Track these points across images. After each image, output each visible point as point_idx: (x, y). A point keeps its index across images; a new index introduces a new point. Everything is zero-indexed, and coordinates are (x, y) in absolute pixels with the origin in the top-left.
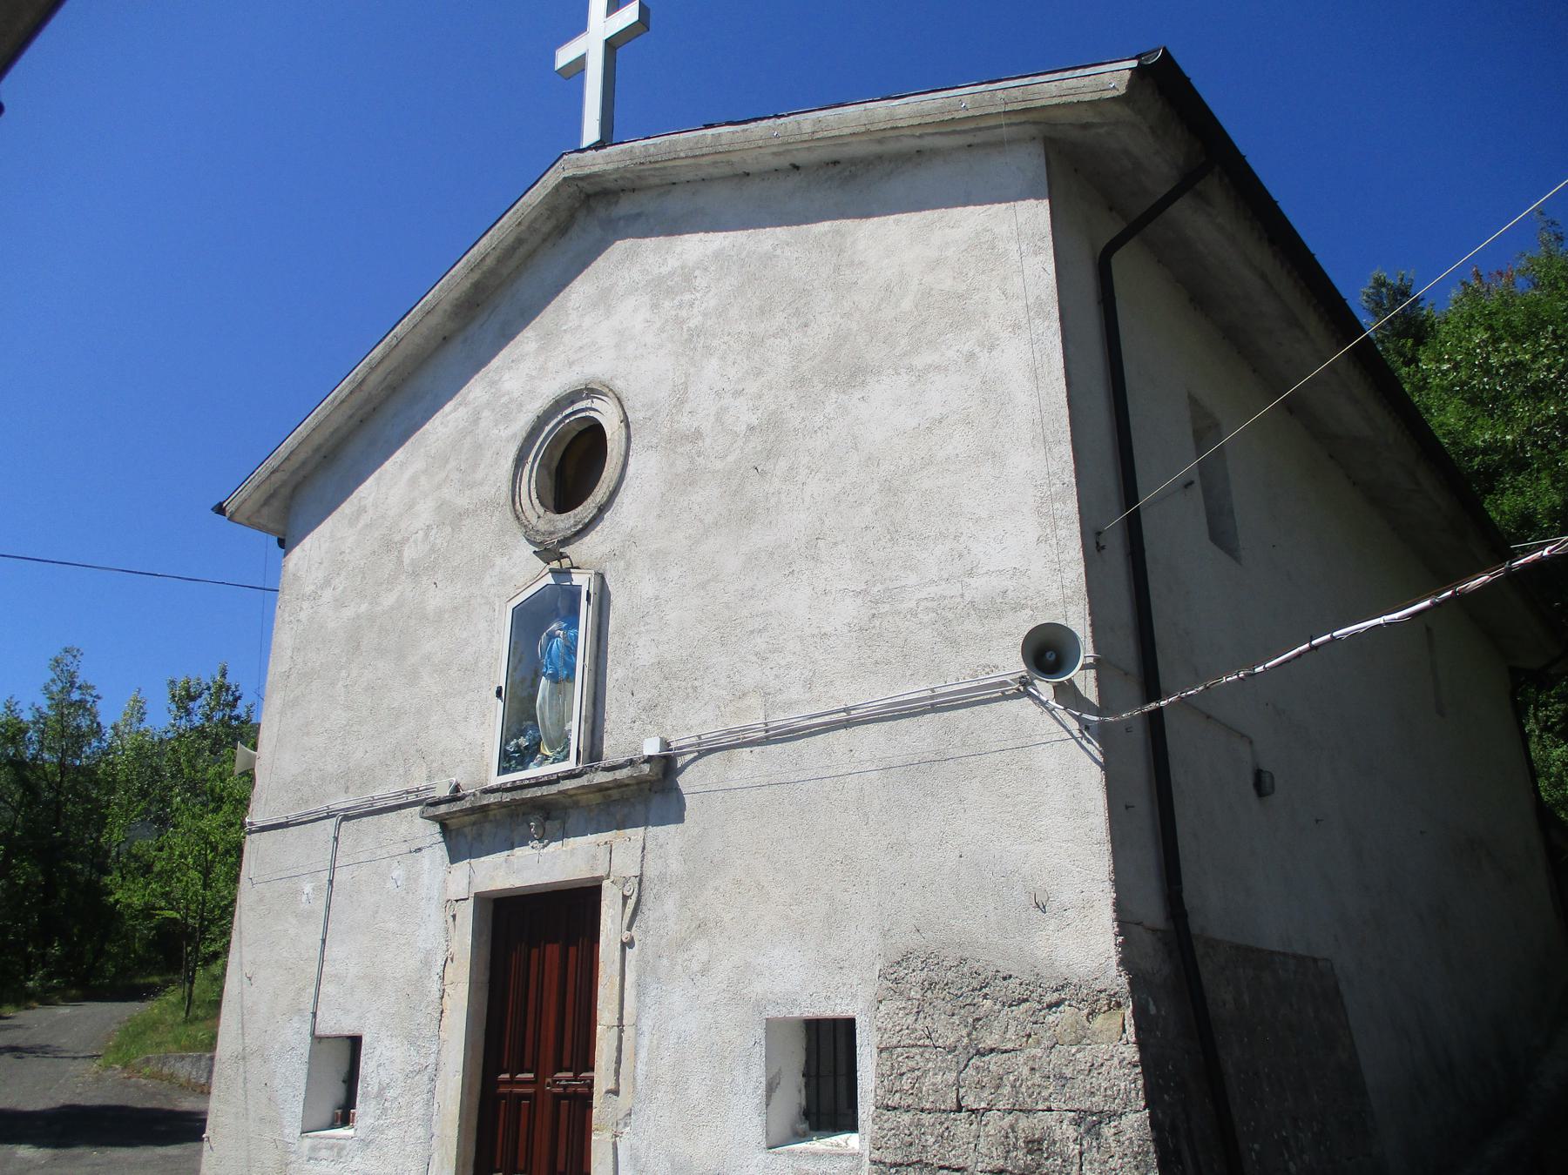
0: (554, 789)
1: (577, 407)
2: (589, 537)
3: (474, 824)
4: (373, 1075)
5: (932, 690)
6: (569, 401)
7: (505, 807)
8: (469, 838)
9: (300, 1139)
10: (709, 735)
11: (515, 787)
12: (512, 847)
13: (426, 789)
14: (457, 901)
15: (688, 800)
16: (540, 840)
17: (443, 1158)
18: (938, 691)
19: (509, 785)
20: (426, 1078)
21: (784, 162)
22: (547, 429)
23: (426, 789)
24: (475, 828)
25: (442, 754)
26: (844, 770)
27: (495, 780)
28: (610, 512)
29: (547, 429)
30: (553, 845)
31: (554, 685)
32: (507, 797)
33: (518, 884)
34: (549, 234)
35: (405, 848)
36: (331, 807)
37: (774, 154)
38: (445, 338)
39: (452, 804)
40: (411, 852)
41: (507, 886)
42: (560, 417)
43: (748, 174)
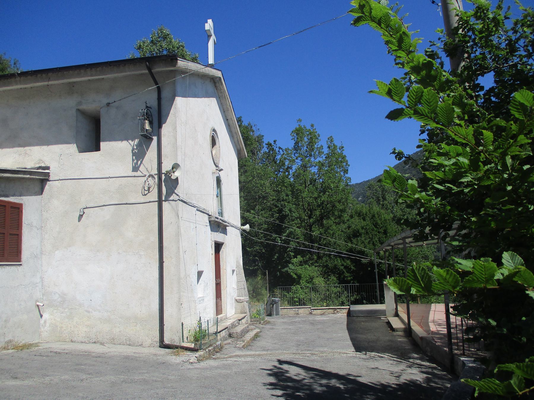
21: (229, 118)
37: (231, 119)
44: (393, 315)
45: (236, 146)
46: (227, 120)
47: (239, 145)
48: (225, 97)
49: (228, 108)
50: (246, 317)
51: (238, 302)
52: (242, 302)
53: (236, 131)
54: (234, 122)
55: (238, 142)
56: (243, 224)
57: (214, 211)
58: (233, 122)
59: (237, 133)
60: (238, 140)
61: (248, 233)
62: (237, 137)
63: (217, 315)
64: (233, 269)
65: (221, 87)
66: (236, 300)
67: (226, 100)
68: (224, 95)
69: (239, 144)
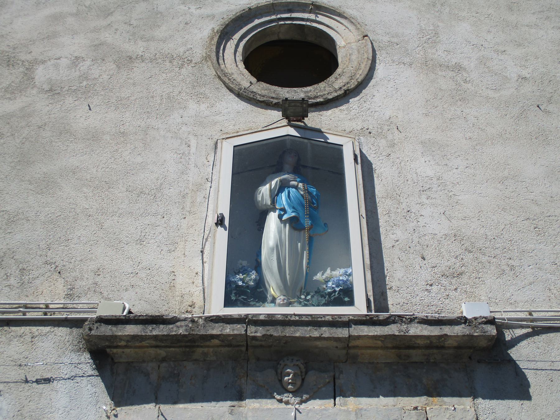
0: (343, 333)
1: (321, 18)
2: (330, 112)
6: (286, 8)
7: (230, 345)
8: (154, 377)
10: (7, 306)
12: (240, 397)
13: (63, 308)
15: (530, 376)
16: (295, 393)
18: (535, 315)
19: (262, 318)
22: (257, 22)
23: (63, 308)
25: (97, 273)
28: (358, 98)
29: (257, 22)
31: (296, 233)
36: (51, 306)
40: (27, 381)
42: (273, 17)
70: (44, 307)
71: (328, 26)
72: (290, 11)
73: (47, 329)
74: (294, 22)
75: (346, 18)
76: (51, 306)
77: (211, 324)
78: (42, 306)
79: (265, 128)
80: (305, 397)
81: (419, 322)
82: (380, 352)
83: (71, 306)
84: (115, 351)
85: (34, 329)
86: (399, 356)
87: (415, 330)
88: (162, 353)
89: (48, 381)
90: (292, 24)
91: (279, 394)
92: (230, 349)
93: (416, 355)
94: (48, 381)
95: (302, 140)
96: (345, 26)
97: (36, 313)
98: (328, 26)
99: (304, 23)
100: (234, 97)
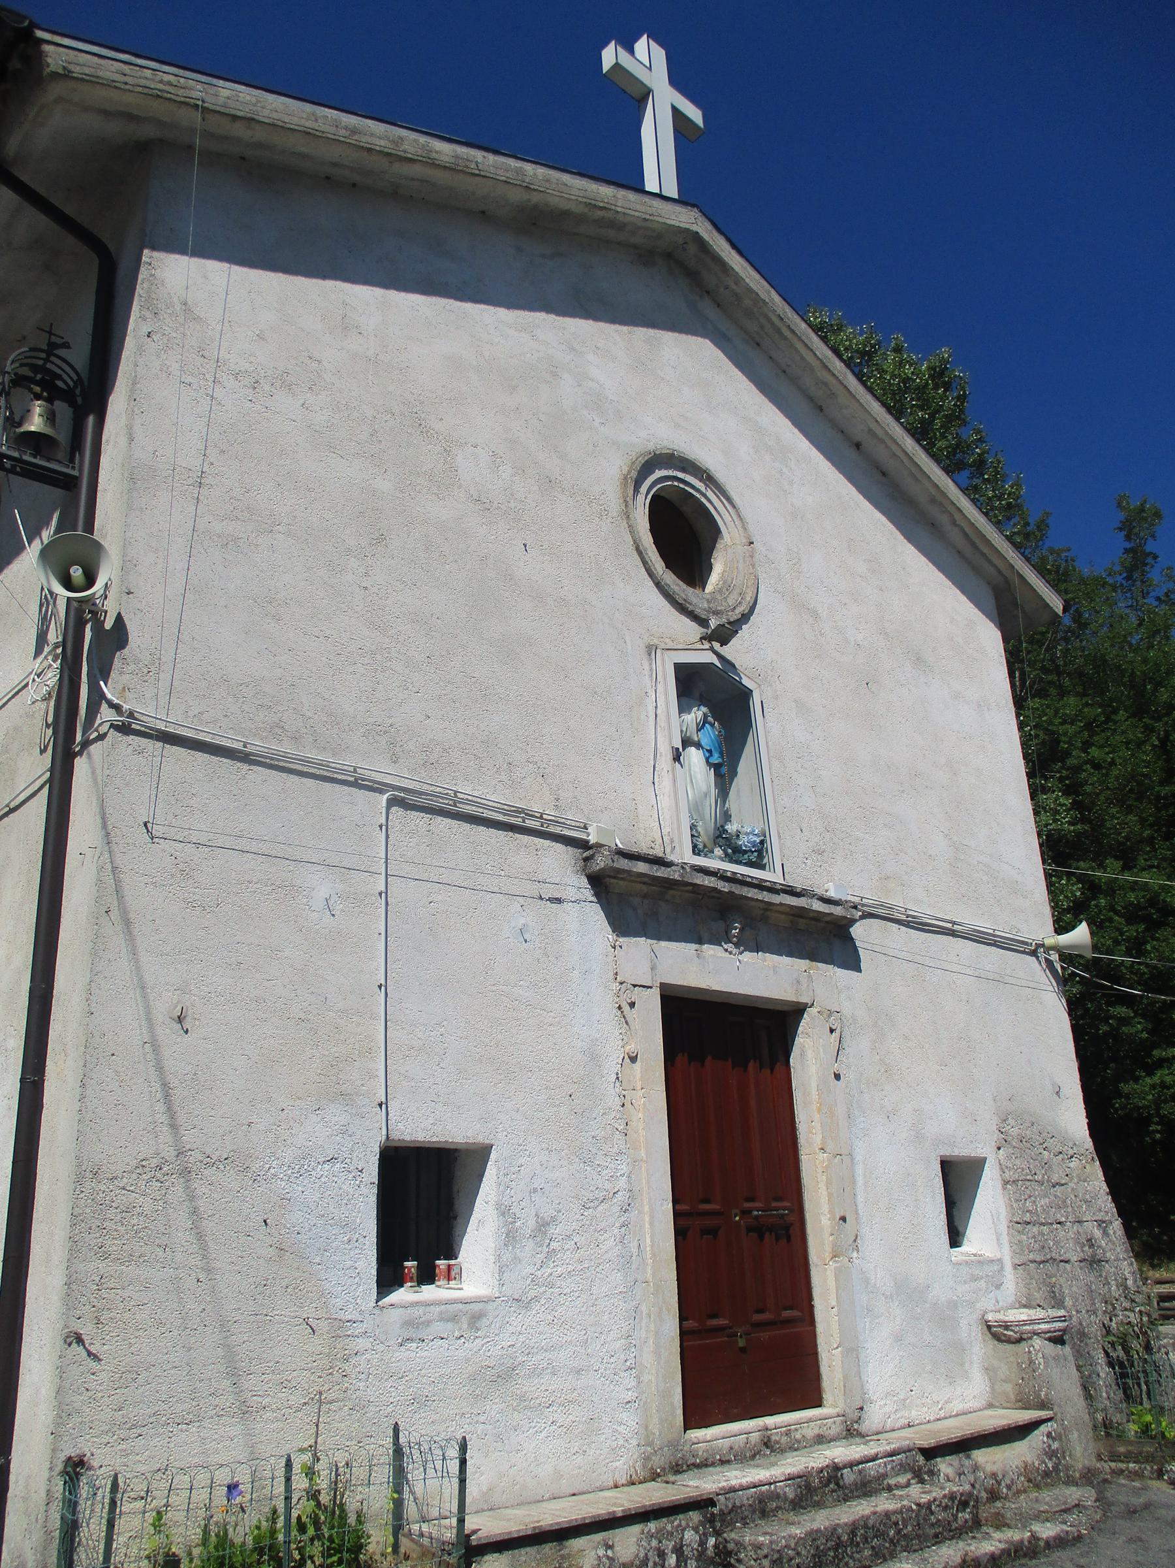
3: (645, 896)
4: (523, 1204)
5: (994, 930)
6: (682, 465)
9: (376, 1311)
11: (733, 879)
14: (634, 986)
16: (737, 945)
17: (661, 1309)
19: (729, 874)
20: (616, 1209)
21: (859, 434)
24: (646, 901)
26: (886, 959)
27: (683, 854)
30: (747, 953)
32: (724, 887)
33: (716, 987)
34: (635, 247)
35: (533, 889)
37: (870, 431)
38: (483, 212)
39: (655, 867)
40: (541, 898)
41: (703, 986)
43: (821, 410)
44: (664, 993)
45: (977, 570)
46: (858, 446)
47: (990, 562)
48: (778, 331)
49: (826, 384)
50: (1044, 1428)
51: (997, 1337)
52: (1019, 1341)
53: (933, 491)
54: (889, 443)
55: (973, 544)
56: (1061, 927)
57: (665, 832)
58: (887, 447)
59: (939, 498)
60: (966, 534)
61: (1093, 965)
62: (954, 523)
63: (687, 1426)
64: (961, 1150)
65: (734, 287)
66: (989, 1327)
67: (792, 346)
68: (769, 320)
69: (984, 555)
70: (352, 769)
71: (715, 508)
72: (684, 470)
73: (547, 843)
74: (686, 488)
75: (734, 507)
76: (545, 816)
77: (695, 873)
78: (536, 814)
79: (689, 647)
80: (742, 948)
81: (817, 899)
82: (783, 916)
83: (333, 765)
84: (612, 881)
85: (537, 840)
86: (791, 922)
87: (817, 906)
88: (645, 888)
89: (559, 901)
90: (684, 489)
91: (725, 943)
92: (691, 895)
93: (802, 923)
94: (559, 901)
95: (722, 672)
96: (732, 517)
97: (533, 823)
98: (715, 508)
99: (698, 495)
100: (653, 585)
